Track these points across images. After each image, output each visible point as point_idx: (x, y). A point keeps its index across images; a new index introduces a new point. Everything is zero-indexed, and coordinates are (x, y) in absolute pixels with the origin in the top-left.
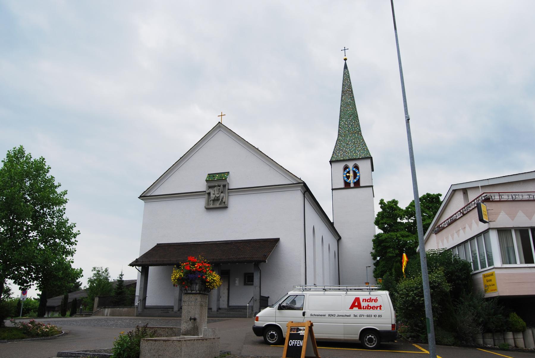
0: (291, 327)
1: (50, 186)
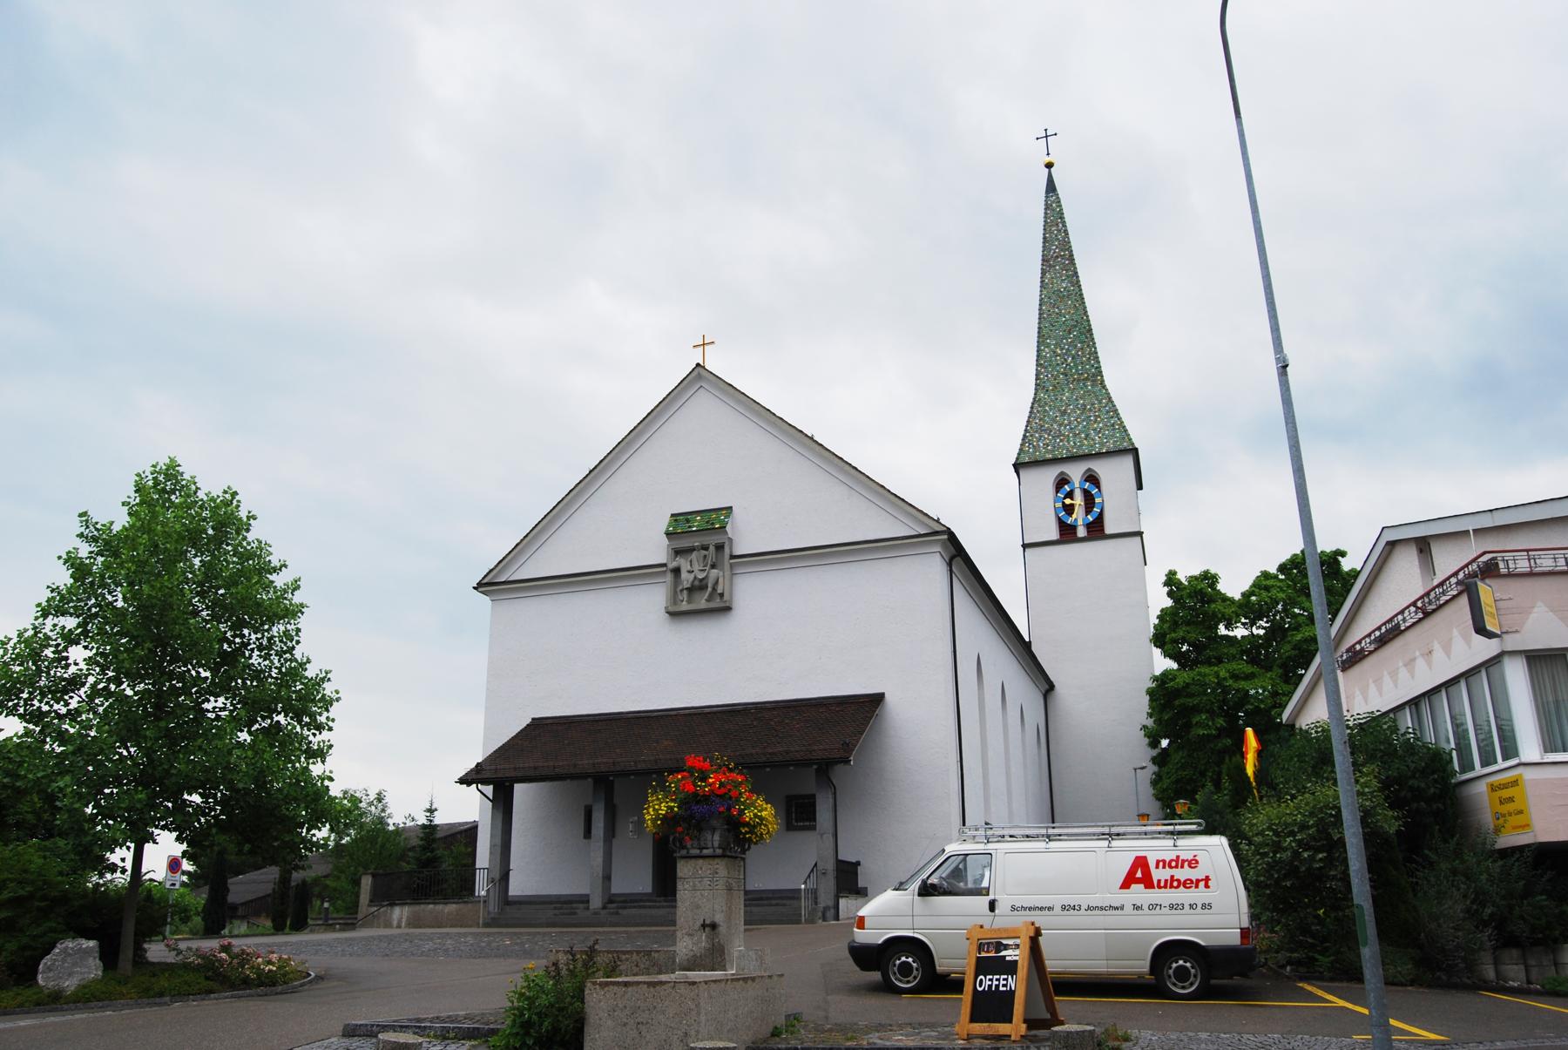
0: (978, 940)
1: (257, 566)
